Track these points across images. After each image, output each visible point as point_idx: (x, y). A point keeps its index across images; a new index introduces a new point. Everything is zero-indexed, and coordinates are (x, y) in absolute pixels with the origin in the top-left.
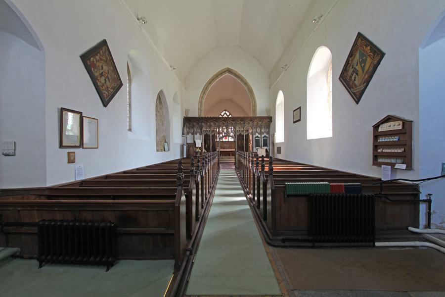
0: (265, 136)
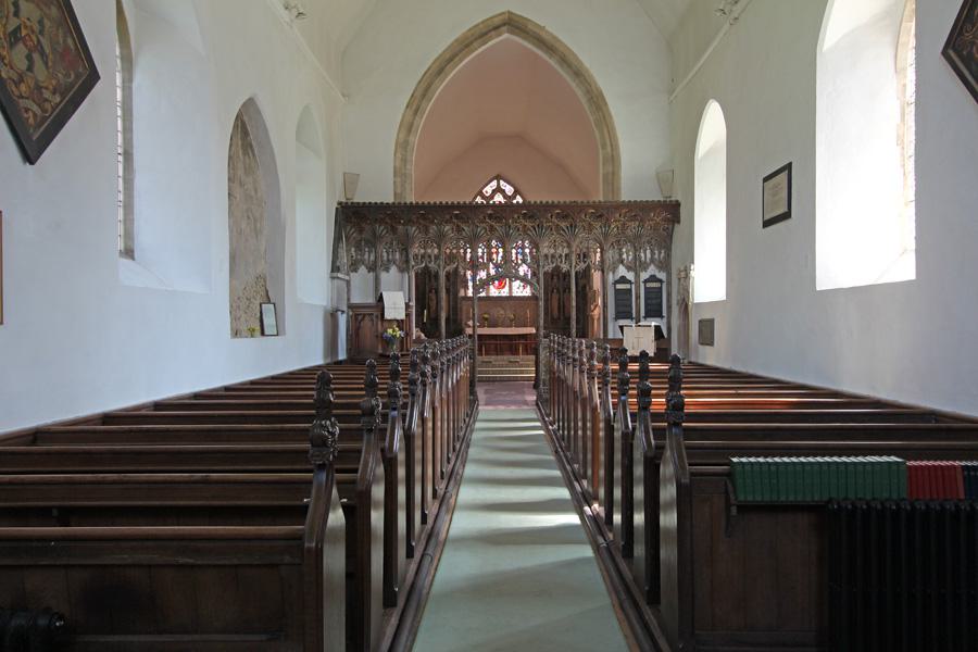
0: (653, 278)
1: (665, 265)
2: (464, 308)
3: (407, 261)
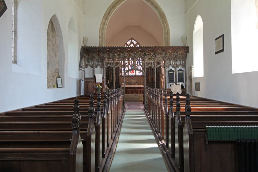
0: (180, 70)
1: (184, 66)
2: (121, 79)
3: (103, 65)
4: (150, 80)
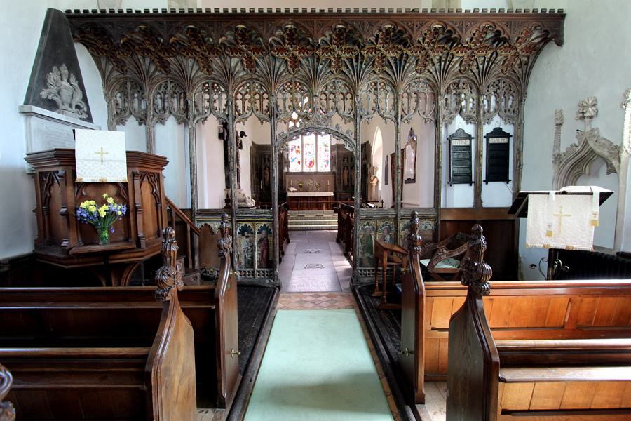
0: (498, 132)
2: (287, 179)
3: (187, 110)
4: (346, 180)
